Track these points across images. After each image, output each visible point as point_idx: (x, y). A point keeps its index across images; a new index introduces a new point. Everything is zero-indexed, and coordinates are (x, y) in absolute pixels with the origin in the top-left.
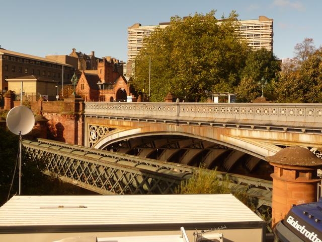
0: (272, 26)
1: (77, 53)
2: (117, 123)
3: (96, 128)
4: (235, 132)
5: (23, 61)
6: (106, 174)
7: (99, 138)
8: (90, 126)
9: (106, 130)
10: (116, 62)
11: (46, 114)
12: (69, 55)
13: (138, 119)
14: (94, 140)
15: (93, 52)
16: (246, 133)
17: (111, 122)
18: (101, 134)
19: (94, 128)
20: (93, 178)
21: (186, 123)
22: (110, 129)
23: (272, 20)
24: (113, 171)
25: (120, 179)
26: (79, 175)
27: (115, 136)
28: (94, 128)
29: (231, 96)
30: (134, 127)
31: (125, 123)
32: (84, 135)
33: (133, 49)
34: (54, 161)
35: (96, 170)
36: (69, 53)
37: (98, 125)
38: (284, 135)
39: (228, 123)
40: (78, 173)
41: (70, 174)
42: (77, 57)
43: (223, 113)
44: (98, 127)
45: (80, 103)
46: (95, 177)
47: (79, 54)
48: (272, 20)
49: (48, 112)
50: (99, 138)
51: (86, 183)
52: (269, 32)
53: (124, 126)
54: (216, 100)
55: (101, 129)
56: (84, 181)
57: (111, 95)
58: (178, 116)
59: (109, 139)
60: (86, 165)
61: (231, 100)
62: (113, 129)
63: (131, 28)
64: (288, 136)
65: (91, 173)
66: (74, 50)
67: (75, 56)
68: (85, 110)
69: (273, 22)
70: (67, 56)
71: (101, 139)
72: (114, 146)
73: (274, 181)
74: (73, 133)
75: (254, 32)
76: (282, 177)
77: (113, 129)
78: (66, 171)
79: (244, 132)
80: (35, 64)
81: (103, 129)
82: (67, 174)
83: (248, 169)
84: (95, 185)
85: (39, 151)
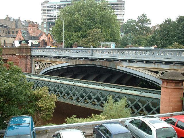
2: (53, 60)
4: (125, 64)
7: (41, 68)
15: (7, 15)
16: (132, 64)
17: (49, 59)
27: (52, 68)
31: (58, 60)
48: (124, 1)
50: (41, 68)
53: (58, 62)
59: (48, 69)
62: (50, 63)
77: (50, 63)
81: (44, 64)
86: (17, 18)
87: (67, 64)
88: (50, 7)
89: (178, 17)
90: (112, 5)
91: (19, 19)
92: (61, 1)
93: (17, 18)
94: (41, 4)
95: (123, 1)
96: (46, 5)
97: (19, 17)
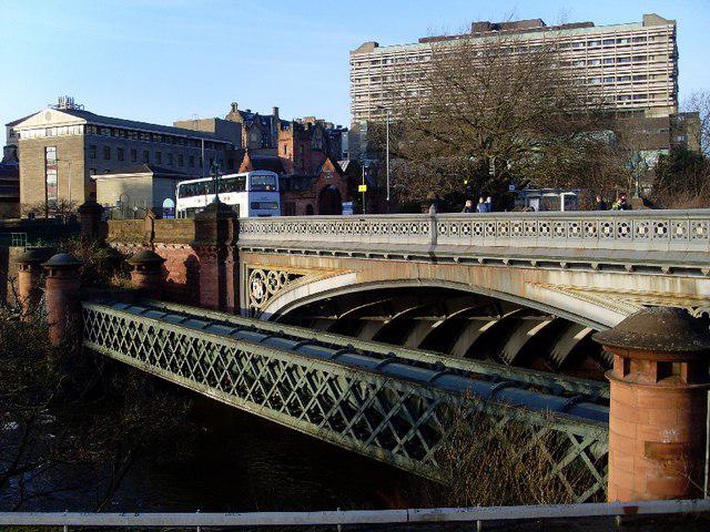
0: (673, 37)
1: (241, 113)
2: (306, 261)
3: (262, 274)
4: (558, 277)
5: (127, 135)
6: (309, 386)
7: (270, 295)
8: (252, 270)
9: (283, 279)
10: (329, 127)
11: (161, 246)
12: (223, 118)
13: (367, 255)
14: (259, 301)
15: (276, 109)
16: (581, 279)
17: (293, 260)
18: (273, 288)
19: (258, 275)
20: (229, 378)
21: (452, 259)
22: (292, 277)
23: (674, 22)
24: (326, 379)
25: (300, 385)
26: (219, 377)
27: (303, 292)
28: (258, 275)
29: (566, 197)
30: (342, 272)
31: (322, 262)
32: (239, 291)
33: (363, 98)
34: (194, 354)
35: (287, 375)
36: (223, 113)
37: (267, 269)
38: (665, 283)
39: (513, 256)
40: (217, 373)
41: (214, 380)
42: (241, 121)
43: (560, 235)
44: (266, 272)
45: (230, 220)
46: (268, 386)
47: (245, 115)
48: (674, 22)
49: (166, 242)
50: (270, 295)
51: (233, 393)
52: (667, 47)
53: (322, 269)
54: (535, 204)
55: (273, 276)
56: (244, 396)
57: (308, 202)
58: (434, 243)
59: (291, 298)
60: (281, 372)
61: (566, 204)
62: (298, 276)
63: (355, 52)
64: (672, 283)
65: (241, 373)
66: (234, 106)
67: (237, 119)
68: (240, 236)
69: (675, 28)
70: (217, 120)
71: (273, 298)
72: (305, 314)
73: (613, 385)
74: (215, 287)
75: (632, 51)
76: (629, 377)
77: (298, 276)
78: (219, 377)
79: (577, 276)
80: (152, 140)
81: (277, 277)
82: (195, 374)
83: (554, 363)
84: (249, 399)
85: (123, 320)
86: (267, 111)
87: (342, 280)
88: (381, 65)
89: (456, 23)
90: (594, 45)
91: (276, 116)
92: (423, 41)
93: (270, 112)
94: (348, 58)
95: (669, 22)
96: (369, 59)
97: (276, 109)
